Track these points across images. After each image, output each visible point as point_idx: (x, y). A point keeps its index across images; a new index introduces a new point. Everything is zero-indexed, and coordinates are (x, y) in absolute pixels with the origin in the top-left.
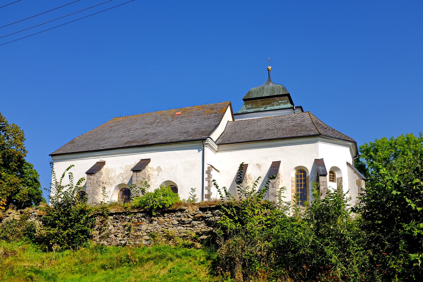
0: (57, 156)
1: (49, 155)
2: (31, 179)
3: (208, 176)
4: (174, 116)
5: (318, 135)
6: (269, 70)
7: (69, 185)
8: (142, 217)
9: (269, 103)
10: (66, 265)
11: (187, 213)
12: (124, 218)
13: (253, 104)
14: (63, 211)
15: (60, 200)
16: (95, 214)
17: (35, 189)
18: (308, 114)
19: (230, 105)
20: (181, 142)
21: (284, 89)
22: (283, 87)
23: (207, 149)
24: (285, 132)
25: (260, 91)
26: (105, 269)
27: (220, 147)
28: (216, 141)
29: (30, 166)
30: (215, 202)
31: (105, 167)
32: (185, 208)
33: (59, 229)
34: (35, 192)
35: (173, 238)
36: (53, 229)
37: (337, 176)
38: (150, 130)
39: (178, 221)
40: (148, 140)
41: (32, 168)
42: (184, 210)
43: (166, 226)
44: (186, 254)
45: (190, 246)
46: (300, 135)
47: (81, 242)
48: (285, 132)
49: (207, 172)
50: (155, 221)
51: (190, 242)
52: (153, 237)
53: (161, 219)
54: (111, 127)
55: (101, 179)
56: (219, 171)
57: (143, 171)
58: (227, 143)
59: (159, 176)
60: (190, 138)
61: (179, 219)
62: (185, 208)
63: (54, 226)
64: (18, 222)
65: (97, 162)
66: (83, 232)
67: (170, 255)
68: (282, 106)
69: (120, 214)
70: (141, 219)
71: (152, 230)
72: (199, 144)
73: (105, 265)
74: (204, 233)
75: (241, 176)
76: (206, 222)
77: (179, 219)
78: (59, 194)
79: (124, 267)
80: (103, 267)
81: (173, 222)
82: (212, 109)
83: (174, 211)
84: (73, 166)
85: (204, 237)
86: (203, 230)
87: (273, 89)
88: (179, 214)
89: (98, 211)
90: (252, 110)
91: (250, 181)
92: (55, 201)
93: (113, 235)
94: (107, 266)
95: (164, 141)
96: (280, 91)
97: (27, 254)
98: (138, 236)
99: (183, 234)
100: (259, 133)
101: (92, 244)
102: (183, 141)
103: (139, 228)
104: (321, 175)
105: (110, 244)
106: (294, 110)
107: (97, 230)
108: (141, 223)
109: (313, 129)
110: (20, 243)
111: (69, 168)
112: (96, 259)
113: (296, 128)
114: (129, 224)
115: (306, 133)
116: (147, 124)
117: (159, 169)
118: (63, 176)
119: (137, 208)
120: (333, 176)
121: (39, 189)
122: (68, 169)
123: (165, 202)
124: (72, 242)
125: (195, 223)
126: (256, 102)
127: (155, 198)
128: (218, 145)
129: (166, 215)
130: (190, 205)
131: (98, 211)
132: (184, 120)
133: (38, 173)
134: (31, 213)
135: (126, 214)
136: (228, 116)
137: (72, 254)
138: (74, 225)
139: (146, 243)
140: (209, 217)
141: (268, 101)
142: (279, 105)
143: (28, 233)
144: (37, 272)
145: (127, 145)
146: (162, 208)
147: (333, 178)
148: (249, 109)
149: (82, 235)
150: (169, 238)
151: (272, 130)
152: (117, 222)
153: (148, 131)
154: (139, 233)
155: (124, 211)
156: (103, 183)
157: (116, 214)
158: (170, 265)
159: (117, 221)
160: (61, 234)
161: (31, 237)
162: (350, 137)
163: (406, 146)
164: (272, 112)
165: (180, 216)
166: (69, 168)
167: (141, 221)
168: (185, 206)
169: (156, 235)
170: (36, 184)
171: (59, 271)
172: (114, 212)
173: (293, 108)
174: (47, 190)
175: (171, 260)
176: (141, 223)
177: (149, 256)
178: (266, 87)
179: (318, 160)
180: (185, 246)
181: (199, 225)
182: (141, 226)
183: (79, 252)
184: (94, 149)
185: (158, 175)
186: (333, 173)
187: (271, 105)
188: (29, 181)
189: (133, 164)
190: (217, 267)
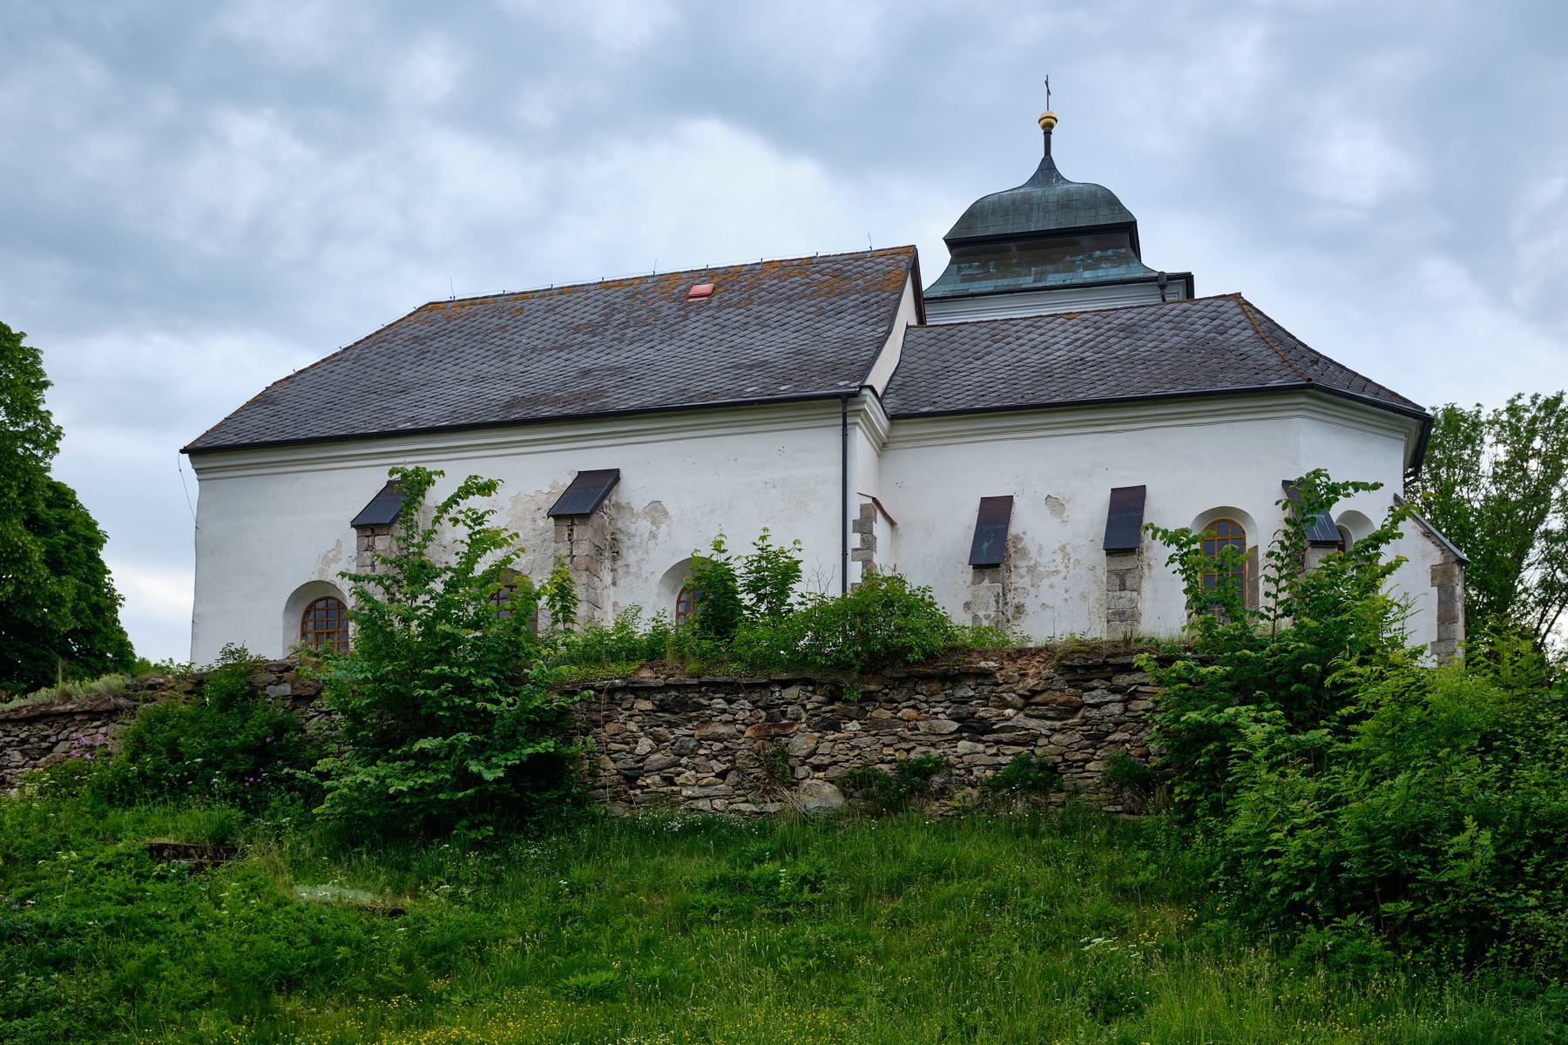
1: (182, 451)
3: (863, 540)
40: (597, 393)
43: (904, 739)
71: (840, 757)
90: (988, 285)
91: (1020, 563)
95: (675, 401)
116: (577, 330)
117: (656, 511)
151: (1098, 364)
152: (671, 725)
165: (964, 701)
176: (785, 727)
185: (653, 536)
187: (1061, 266)
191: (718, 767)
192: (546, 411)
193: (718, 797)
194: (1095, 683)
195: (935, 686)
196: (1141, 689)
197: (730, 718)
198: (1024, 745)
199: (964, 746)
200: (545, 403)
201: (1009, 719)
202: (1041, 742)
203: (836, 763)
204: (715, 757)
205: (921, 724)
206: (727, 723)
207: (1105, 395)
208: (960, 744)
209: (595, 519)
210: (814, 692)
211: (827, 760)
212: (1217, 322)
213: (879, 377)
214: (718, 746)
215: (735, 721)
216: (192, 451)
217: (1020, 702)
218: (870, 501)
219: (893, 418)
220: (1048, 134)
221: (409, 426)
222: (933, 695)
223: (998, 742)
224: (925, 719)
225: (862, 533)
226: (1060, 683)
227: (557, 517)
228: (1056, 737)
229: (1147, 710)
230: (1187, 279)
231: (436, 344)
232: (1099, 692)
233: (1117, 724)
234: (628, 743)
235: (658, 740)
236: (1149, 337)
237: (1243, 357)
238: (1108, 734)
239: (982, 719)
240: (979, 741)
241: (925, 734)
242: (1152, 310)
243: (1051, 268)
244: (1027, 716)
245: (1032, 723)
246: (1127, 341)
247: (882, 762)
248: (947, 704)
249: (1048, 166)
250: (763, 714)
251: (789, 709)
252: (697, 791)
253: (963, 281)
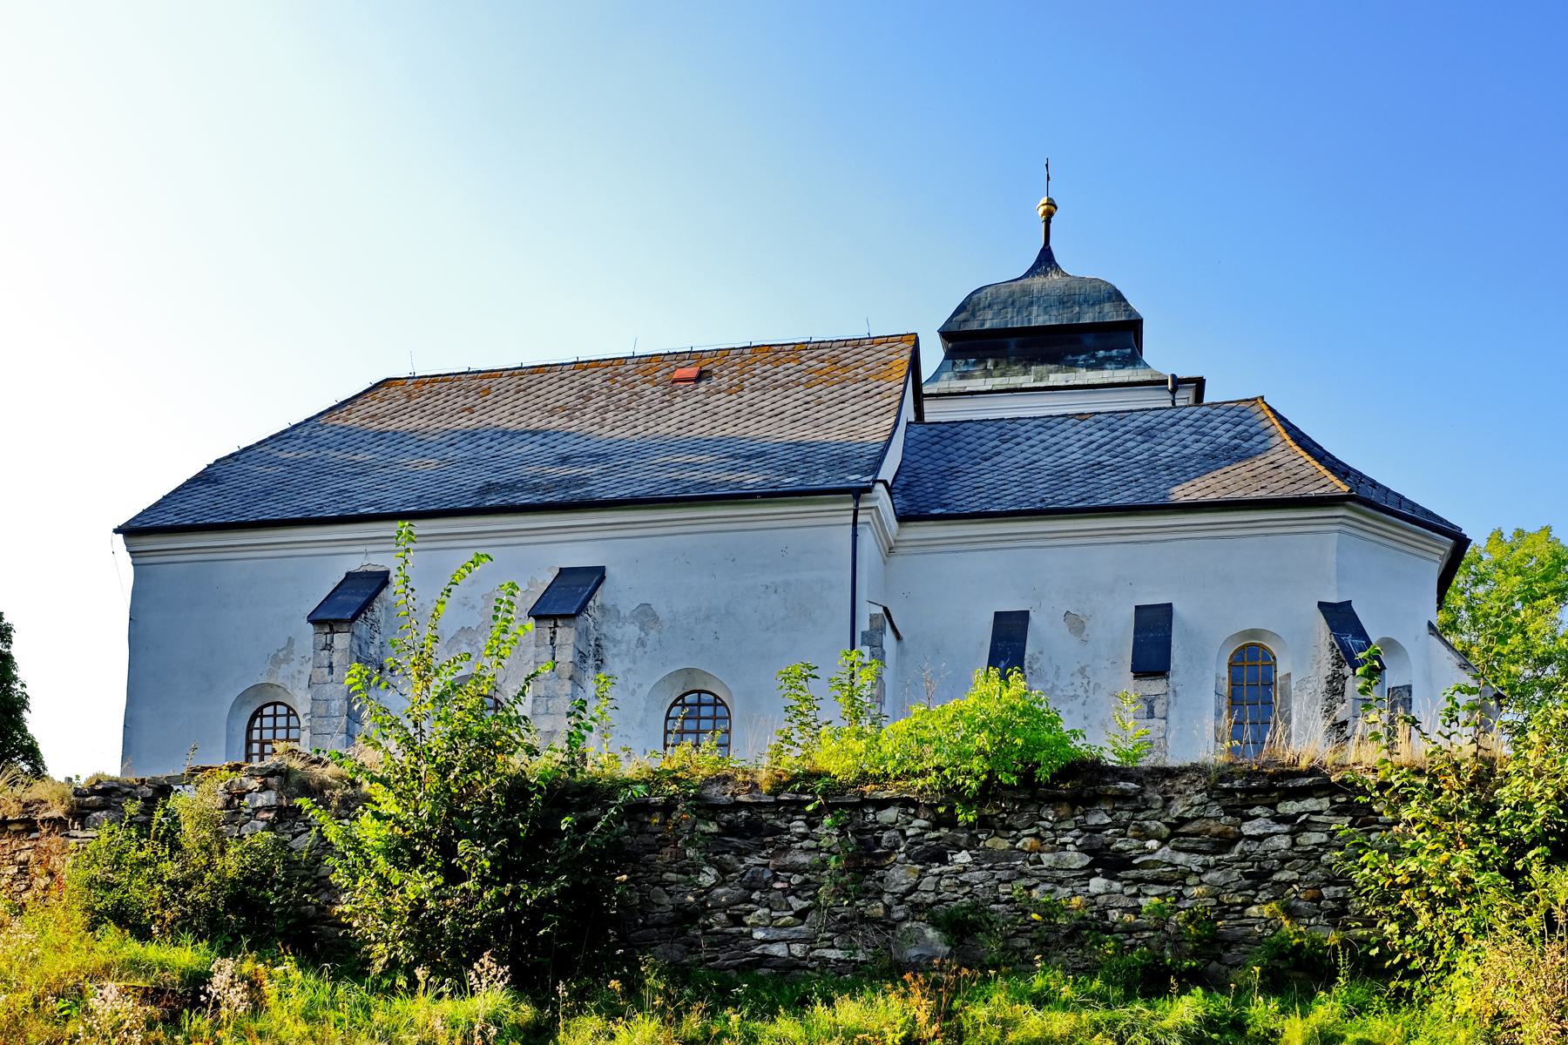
1: (116, 531)
43: (1022, 875)
59: (648, 649)
90: (990, 384)
95: (665, 492)
102: (764, 495)
115: (1290, 492)
145: (494, 500)
165: (1099, 829)
191: (797, 904)
192: (524, 498)
193: (798, 941)
194: (1257, 810)
195: (1064, 810)
196: (1314, 818)
197: (813, 844)
198: (1169, 883)
199: (1097, 884)
200: (522, 489)
201: (1152, 852)
202: (1191, 880)
203: (941, 902)
204: (794, 893)
205: (1044, 857)
206: (809, 850)
208: (1093, 881)
209: (580, 619)
210: (916, 816)
211: (931, 898)
212: (1241, 428)
213: (888, 471)
214: (796, 879)
215: (818, 849)
216: (130, 531)
217: (1166, 831)
218: (881, 610)
219: (903, 518)
220: (1048, 222)
221: (372, 510)
222: (1059, 821)
223: (1137, 881)
224: (1053, 851)
226: (1215, 810)
227: (538, 618)
228: (1213, 875)
229: (1319, 845)
230: (1199, 384)
232: (1261, 821)
233: (1283, 861)
234: (687, 873)
235: (723, 870)
236: (1169, 442)
238: (1272, 872)
239: (1120, 851)
240: (1115, 879)
241: (1050, 869)
243: (1052, 367)
244: (1175, 849)
245: (1181, 858)
246: (1146, 446)
247: (997, 901)
248: (1076, 832)
249: (1046, 259)
251: (885, 835)
252: (773, 934)
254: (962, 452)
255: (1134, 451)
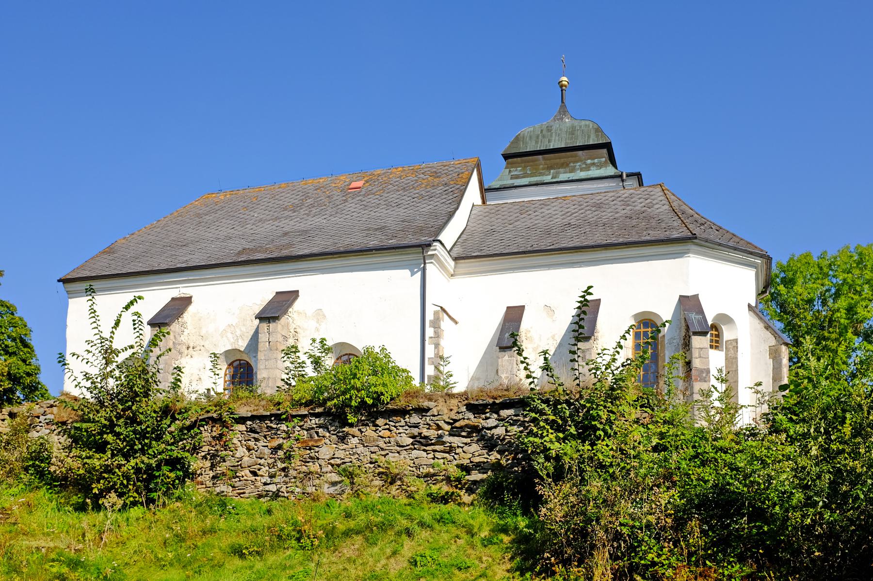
0: (84, 282)
1: (59, 281)
2: (14, 340)
4: (347, 192)
5: (690, 239)
6: (561, 86)
7: (132, 347)
8: (320, 427)
9: (564, 165)
10: (140, 545)
11: (435, 418)
12: (272, 428)
13: (525, 167)
14: (123, 410)
15: (111, 383)
16: (202, 420)
17: (24, 361)
18: (659, 189)
19: (478, 166)
20: (371, 250)
21: (598, 130)
22: (596, 126)
23: (431, 268)
24: (609, 232)
25: (544, 137)
26: (242, 556)
27: (459, 265)
28: (451, 249)
29: (8, 307)
30: (507, 390)
31: (191, 309)
32: (431, 404)
33: (113, 455)
34: (24, 368)
35: (400, 479)
36: (98, 456)
37: (727, 334)
38: (292, 223)
39: (413, 437)
40: (290, 245)
41: (12, 314)
42: (429, 409)
43: (382, 449)
44: (441, 520)
45: (445, 499)
46: (648, 238)
47: (168, 489)
48: (609, 232)
49: (430, 323)
50: (354, 437)
51: (445, 488)
52: (351, 476)
53: (369, 431)
54: (199, 216)
55: (182, 338)
56: (456, 323)
57: (283, 320)
58: (474, 254)
60: (393, 242)
61: (415, 431)
62: (431, 404)
63: (101, 448)
64: (5, 437)
65: (173, 299)
66: (174, 463)
67: (405, 523)
68: (594, 172)
69: (262, 418)
70: (317, 433)
71: (347, 460)
72: (413, 256)
73: (240, 546)
74: (480, 467)
75: (581, 323)
76: (482, 438)
77: (415, 431)
78: (109, 369)
79: (288, 552)
80: (238, 552)
81: (398, 439)
82: (436, 175)
83: (403, 412)
84: (140, 298)
85: (476, 476)
86: (477, 460)
87: (572, 131)
88: (415, 419)
89: (208, 412)
92: (99, 386)
93: (247, 472)
94: (247, 548)
96: (589, 137)
97: (39, 516)
98: (311, 473)
99: (424, 470)
100: (548, 233)
101: (195, 491)
102: (376, 250)
103: (312, 455)
104: (695, 333)
105: (239, 494)
106: (623, 181)
107: (205, 457)
108: (316, 441)
109: (675, 224)
110: (14, 490)
111: (132, 303)
112: (212, 531)
113: (634, 222)
114: (286, 445)
115: (662, 235)
116: (285, 209)
117: (320, 315)
118: (117, 323)
119: (307, 404)
120: (718, 336)
121: (33, 361)
122: (127, 308)
123: (380, 389)
124: (147, 487)
125: (456, 441)
126: (533, 161)
127: (356, 380)
128: (456, 259)
129: (380, 421)
130: (442, 397)
131: (208, 412)
132: (372, 199)
133: (29, 325)
134: (38, 417)
135: (278, 418)
136: (473, 194)
137: (149, 516)
138: (150, 447)
139: (332, 490)
140: (490, 429)
141: (562, 160)
142: (588, 168)
143: (33, 465)
144: (74, 564)
146: (374, 405)
147: (717, 342)
148: (517, 177)
149: (171, 471)
150: (390, 478)
151: (579, 226)
152: (257, 440)
153: (288, 225)
154: (314, 467)
155: (275, 412)
156: (188, 348)
157: (253, 418)
158: (408, 548)
159: (256, 436)
160: (119, 467)
161: (41, 474)
162: (758, 246)
163: (857, 272)
164: (571, 183)
165: (416, 426)
166: (132, 303)
167: (316, 438)
168: (430, 400)
169: (357, 471)
170: (26, 350)
171: (126, 560)
172: (249, 415)
173: (621, 176)
174: (80, 358)
175: (409, 533)
176: (316, 441)
177: (352, 524)
178: (556, 125)
179: (688, 297)
180: (435, 499)
181: (466, 448)
182: (317, 449)
183: (166, 511)
184: (164, 266)
186: (717, 330)
187: (568, 169)
188: (9, 342)
189: (259, 302)
190: (528, 551)
207: (578, 244)
212: (649, 201)
221: (184, 265)
225: (435, 328)
231: (207, 217)
236: (609, 210)
237: (660, 221)
242: (612, 194)
243: (561, 170)
246: (596, 213)
248: (407, 427)
250: (305, 432)
253: (511, 178)
254: (499, 220)
255: (590, 216)
